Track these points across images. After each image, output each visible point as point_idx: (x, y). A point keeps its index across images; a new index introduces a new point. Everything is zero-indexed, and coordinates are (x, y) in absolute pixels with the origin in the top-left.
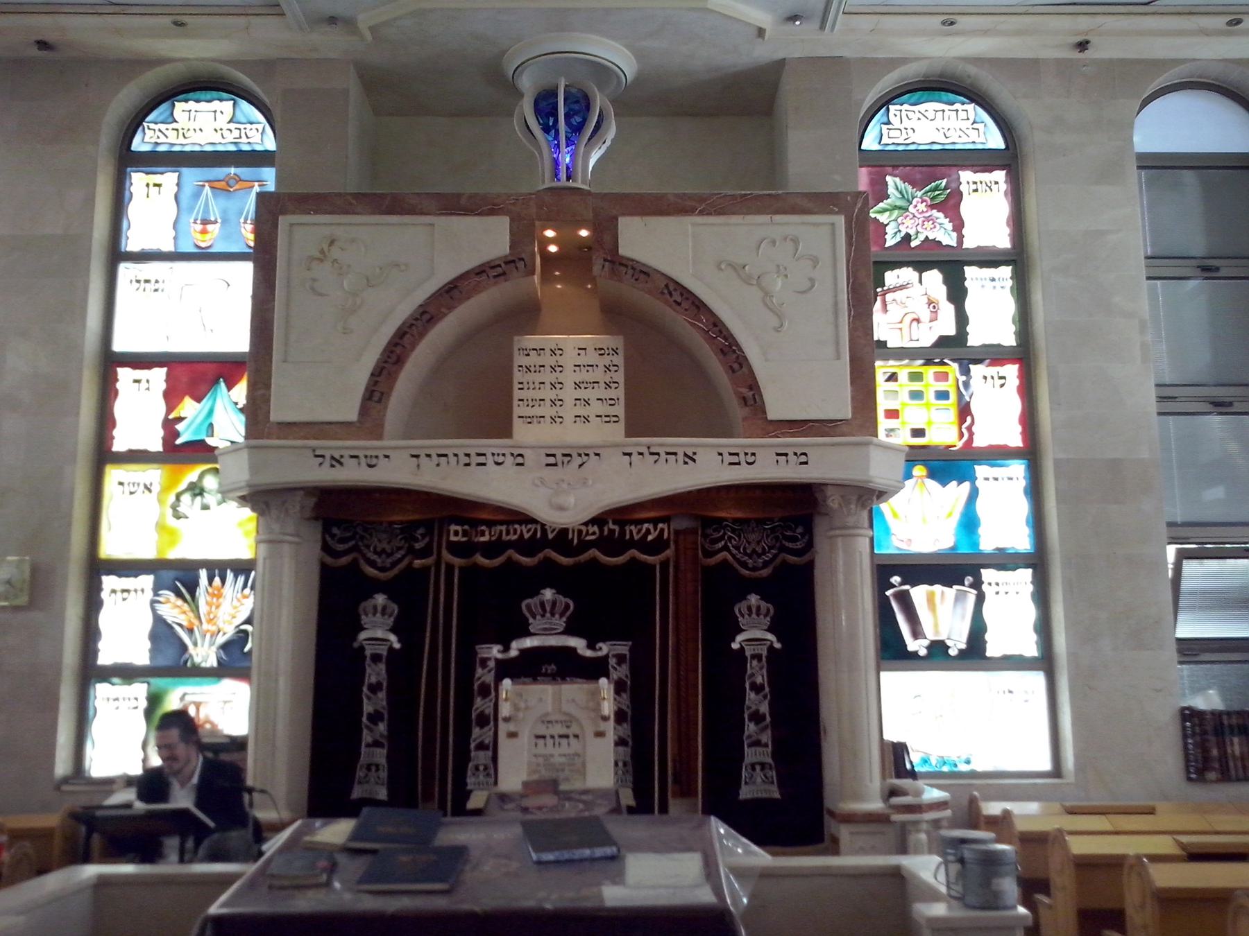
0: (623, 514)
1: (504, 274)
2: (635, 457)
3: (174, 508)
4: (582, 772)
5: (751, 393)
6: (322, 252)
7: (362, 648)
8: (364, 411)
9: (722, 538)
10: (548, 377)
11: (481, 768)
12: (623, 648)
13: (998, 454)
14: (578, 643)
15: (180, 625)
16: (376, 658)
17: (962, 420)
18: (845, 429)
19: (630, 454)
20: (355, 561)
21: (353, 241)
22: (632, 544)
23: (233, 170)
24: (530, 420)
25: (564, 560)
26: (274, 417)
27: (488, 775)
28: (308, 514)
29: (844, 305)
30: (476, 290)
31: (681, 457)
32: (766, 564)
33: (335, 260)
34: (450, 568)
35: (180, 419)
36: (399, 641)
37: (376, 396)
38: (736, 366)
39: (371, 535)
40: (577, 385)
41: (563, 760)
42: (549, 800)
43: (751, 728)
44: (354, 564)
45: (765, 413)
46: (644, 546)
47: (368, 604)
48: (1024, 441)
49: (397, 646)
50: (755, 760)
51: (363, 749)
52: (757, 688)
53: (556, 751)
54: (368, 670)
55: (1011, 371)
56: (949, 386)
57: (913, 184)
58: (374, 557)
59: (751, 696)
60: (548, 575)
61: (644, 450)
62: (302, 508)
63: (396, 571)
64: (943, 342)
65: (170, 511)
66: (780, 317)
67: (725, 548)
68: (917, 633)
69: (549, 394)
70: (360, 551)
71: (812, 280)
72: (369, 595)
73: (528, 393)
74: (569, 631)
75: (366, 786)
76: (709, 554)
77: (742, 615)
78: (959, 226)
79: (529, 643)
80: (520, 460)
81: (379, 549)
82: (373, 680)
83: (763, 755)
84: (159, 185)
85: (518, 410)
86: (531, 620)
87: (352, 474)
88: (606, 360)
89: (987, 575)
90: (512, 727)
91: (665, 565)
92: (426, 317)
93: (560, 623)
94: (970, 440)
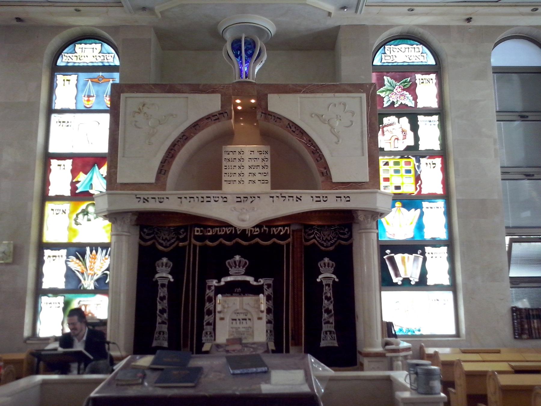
0: (270, 223)
1: (218, 119)
2: (275, 198)
3: (75, 220)
4: (252, 335)
5: (325, 171)
6: (140, 109)
7: (157, 281)
8: (158, 178)
9: (313, 234)
10: (237, 164)
11: (209, 333)
12: (270, 281)
13: (432, 197)
14: (250, 279)
15: (78, 271)
16: (163, 285)
17: (417, 182)
18: (366, 186)
19: (273, 197)
20: (154, 243)
21: (153, 104)
22: (274, 236)
23: (101, 74)
24: (229, 182)
25: (244, 243)
26: (119, 181)
27: (211, 336)
28: (133, 223)
29: (366, 132)
30: (206, 126)
31: (295, 198)
32: (332, 245)
33: (145, 113)
34: (195, 246)
35: (78, 182)
36: (173, 278)
37: (163, 172)
38: (319, 159)
39: (161, 232)
40: (250, 167)
41: (244, 329)
42: (238, 347)
43: (325, 316)
44: (154, 245)
45: (331, 179)
46: (279, 237)
47: (159, 262)
48: (444, 191)
49: (172, 280)
50: (327, 330)
51: (157, 325)
52: (328, 299)
53: (241, 326)
54: (160, 291)
55: (438, 161)
56: (411, 167)
57: (396, 80)
58: (162, 242)
59: (325, 302)
60: (237, 249)
61: (279, 195)
62: (131, 220)
63: (171, 248)
64: (408, 148)
65: (74, 222)
66: (338, 137)
67: (314, 238)
68: (397, 275)
69: (238, 171)
70: (156, 239)
71: (352, 122)
72: (160, 258)
73: (229, 171)
74: (246, 274)
75: (159, 341)
76: (307, 240)
77: (322, 267)
78: (415, 98)
79: (229, 279)
80: (225, 199)
81: (164, 238)
82: (162, 295)
83: (330, 327)
84: (69, 80)
85: (224, 178)
86: (230, 269)
87: (153, 206)
88: (263, 156)
89: (428, 249)
90: (222, 315)
91: (288, 245)
92: (185, 137)
93: (243, 270)
94: (420, 191)
